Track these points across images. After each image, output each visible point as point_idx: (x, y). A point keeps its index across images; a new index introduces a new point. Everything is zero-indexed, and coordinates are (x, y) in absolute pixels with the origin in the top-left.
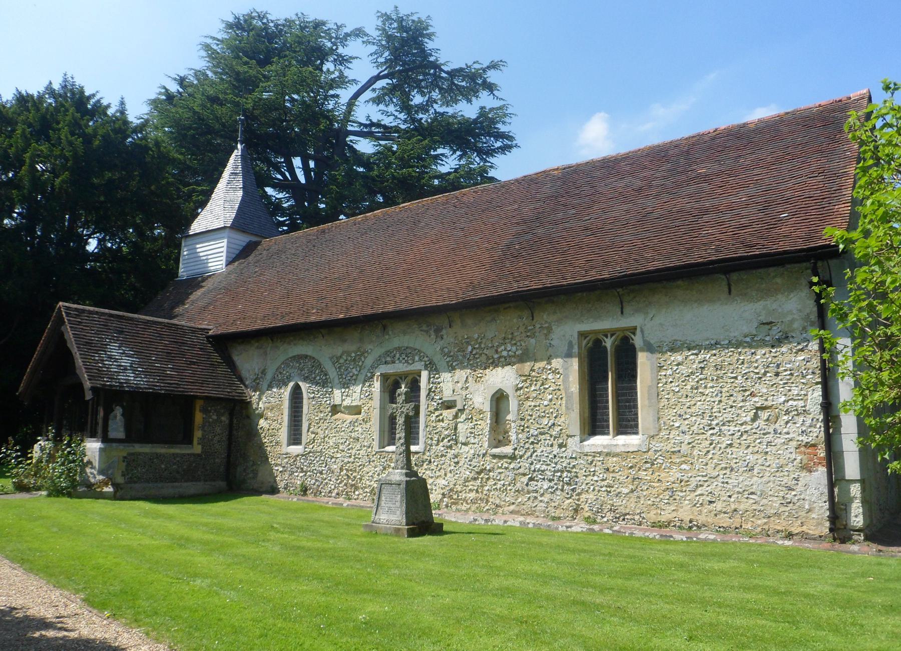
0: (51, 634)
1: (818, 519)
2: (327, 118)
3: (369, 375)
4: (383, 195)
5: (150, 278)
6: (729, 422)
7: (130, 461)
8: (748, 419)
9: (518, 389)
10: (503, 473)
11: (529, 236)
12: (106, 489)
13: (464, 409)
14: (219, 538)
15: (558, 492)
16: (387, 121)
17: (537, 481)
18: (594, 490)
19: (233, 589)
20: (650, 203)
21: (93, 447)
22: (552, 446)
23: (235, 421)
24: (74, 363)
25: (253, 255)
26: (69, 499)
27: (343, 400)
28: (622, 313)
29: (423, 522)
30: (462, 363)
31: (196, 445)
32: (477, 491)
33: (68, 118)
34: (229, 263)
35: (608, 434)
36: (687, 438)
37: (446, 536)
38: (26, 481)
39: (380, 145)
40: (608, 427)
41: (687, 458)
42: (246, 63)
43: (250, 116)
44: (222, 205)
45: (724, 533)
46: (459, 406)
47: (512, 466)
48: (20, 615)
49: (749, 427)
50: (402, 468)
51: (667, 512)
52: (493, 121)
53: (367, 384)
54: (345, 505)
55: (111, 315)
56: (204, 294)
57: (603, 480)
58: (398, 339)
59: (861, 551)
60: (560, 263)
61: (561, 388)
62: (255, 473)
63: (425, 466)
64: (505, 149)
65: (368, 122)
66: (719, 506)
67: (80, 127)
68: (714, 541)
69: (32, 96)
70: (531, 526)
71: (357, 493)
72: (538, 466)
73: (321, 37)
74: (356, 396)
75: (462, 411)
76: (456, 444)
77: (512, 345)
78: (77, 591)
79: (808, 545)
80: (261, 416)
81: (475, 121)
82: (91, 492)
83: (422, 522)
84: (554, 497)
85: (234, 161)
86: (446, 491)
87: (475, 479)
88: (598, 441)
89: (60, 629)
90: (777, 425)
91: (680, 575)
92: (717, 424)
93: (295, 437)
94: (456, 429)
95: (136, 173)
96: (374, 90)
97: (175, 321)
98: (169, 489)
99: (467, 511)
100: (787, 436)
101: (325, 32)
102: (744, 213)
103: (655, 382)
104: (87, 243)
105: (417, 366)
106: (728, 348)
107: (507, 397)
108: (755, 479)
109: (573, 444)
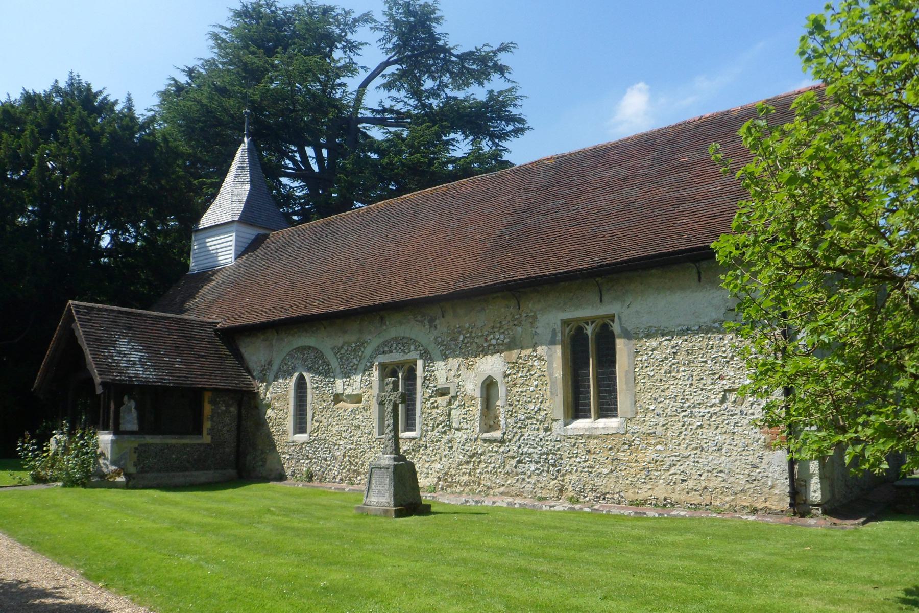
0: (49, 601)
1: (780, 497)
2: (335, 107)
3: (368, 364)
4: (397, 183)
5: (162, 273)
6: (699, 404)
7: (142, 452)
8: (717, 401)
9: (506, 376)
10: (493, 457)
11: (520, 227)
12: (118, 479)
13: (457, 396)
14: (218, 521)
15: (545, 474)
16: (399, 107)
17: (525, 463)
18: (577, 471)
19: (217, 563)
20: (633, 193)
21: (105, 439)
22: (538, 430)
23: (243, 412)
24: (85, 358)
25: (261, 248)
26: (83, 489)
27: (344, 389)
28: (601, 301)
29: (411, 503)
30: (454, 351)
31: (205, 435)
32: (470, 475)
33: (74, 117)
34: (238, 256)
35: (590, 417)
36: (662, 420)
37: (432, 516)
38: (43, 473)
39: (390, 132)
40: (590, 410)
41: (661, 439)
42: (253, 53)
43: (256, 108)
44: (230, 198)
45: (695, 509)
46: (452, 393)
47: (501, 450)
48: (25, 587)
49: (718, 409)
50: (391, 453)
51: (643, 491)
52: (504, 105)
53: (367, 373)
54: (347, 490)
55: (120, 312)
56: (214, 287)
57: (585, 461)
58: (395, 330)
59: (817, 524)
60: (545, 253)
61: (546, 374)
62: (264, 461)
63: (422, 451)
64: (517, 132)
65: (380, 108)
66: (690, 484)
67: (88, 125)
68: (684, 517)
69: (39, 95)
70: (517, 506)
71: (359, 478)
72: (525, 450)
73: (330, 23)
74: (357, 385)
75: (455, 397)
76: (450, 430)
77: (501, 334)
78: (78, 567)
79: (769, 519)
80: (268, 406)
81: (484, 105)
82: (104, 482)
83: (409, 502)
84: (541, 478)
85: (241, 154)
86: (441, 475)
87: (468, 463)
88: (581, 424)
89: (58, 597)
90: (744, 406)
91: (632, 547)
92: (689, 407)
93: (300, 427)
94: (449, 415)
95: (146, 168)
96: (384, 76)
97: (184, 316)
98: (180, 478)
99: (461, 493)
100: (752, 417)
101: (334, 18)
102: (718, 202)
103: (632, 367)
104: (100, 239)
105: (413, 355)
106: (698, 334)
107: (496, 383)
108: (724, 458)
109: (557, 427)
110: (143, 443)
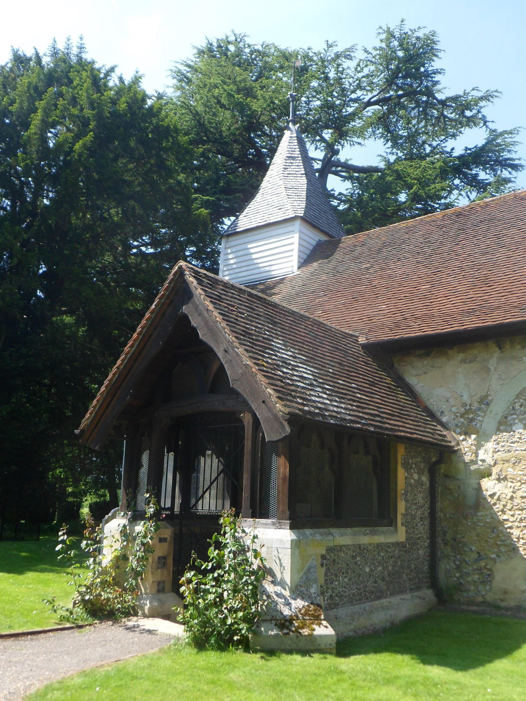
34: (304, 263)
62: (487, 577)
110: (331, 544)
